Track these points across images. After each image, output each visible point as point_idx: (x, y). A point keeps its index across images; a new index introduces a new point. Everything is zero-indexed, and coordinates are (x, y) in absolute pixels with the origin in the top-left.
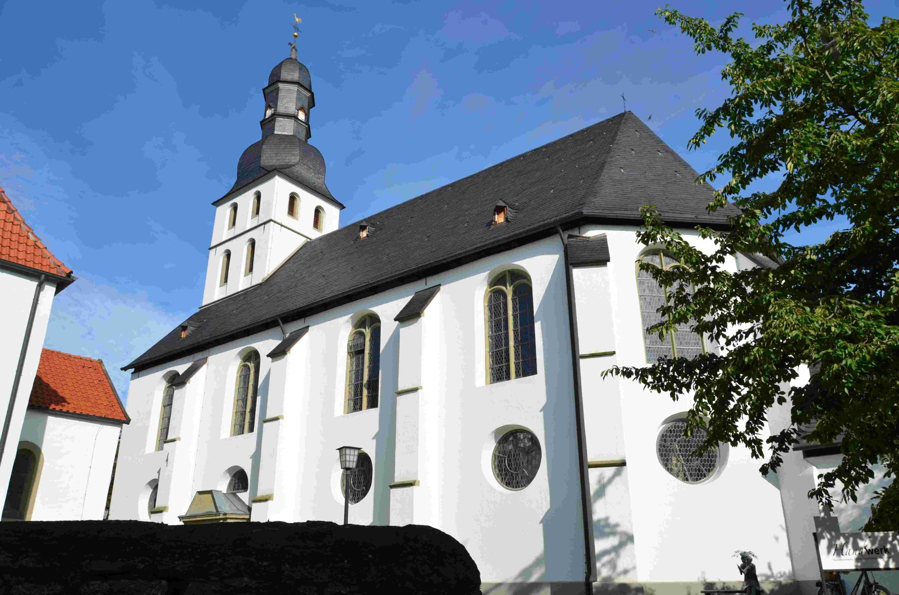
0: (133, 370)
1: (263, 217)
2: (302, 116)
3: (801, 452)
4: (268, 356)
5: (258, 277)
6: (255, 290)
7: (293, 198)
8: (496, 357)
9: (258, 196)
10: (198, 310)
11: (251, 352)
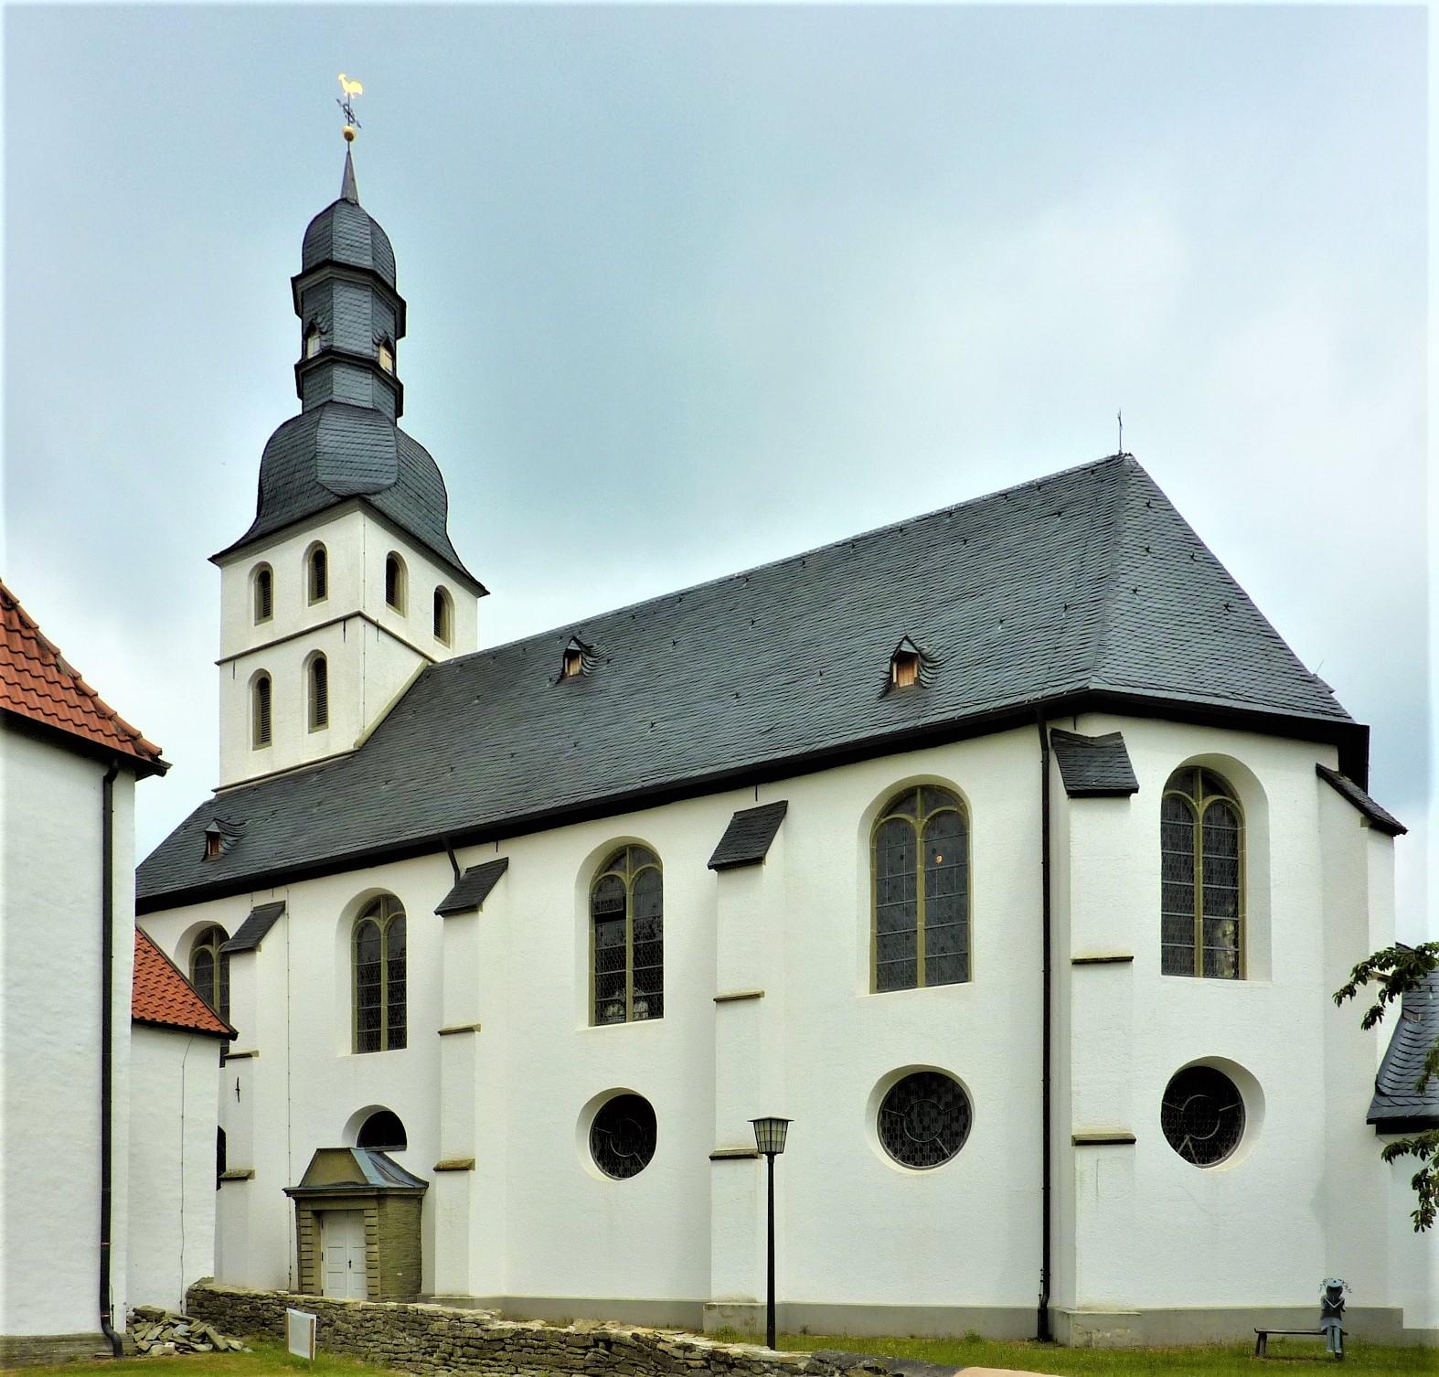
2: (385, 361)
3: (1374, 1126)
5: (343, 735)
7: (393, 566)
9: (318, 558)
10: (212, 796)
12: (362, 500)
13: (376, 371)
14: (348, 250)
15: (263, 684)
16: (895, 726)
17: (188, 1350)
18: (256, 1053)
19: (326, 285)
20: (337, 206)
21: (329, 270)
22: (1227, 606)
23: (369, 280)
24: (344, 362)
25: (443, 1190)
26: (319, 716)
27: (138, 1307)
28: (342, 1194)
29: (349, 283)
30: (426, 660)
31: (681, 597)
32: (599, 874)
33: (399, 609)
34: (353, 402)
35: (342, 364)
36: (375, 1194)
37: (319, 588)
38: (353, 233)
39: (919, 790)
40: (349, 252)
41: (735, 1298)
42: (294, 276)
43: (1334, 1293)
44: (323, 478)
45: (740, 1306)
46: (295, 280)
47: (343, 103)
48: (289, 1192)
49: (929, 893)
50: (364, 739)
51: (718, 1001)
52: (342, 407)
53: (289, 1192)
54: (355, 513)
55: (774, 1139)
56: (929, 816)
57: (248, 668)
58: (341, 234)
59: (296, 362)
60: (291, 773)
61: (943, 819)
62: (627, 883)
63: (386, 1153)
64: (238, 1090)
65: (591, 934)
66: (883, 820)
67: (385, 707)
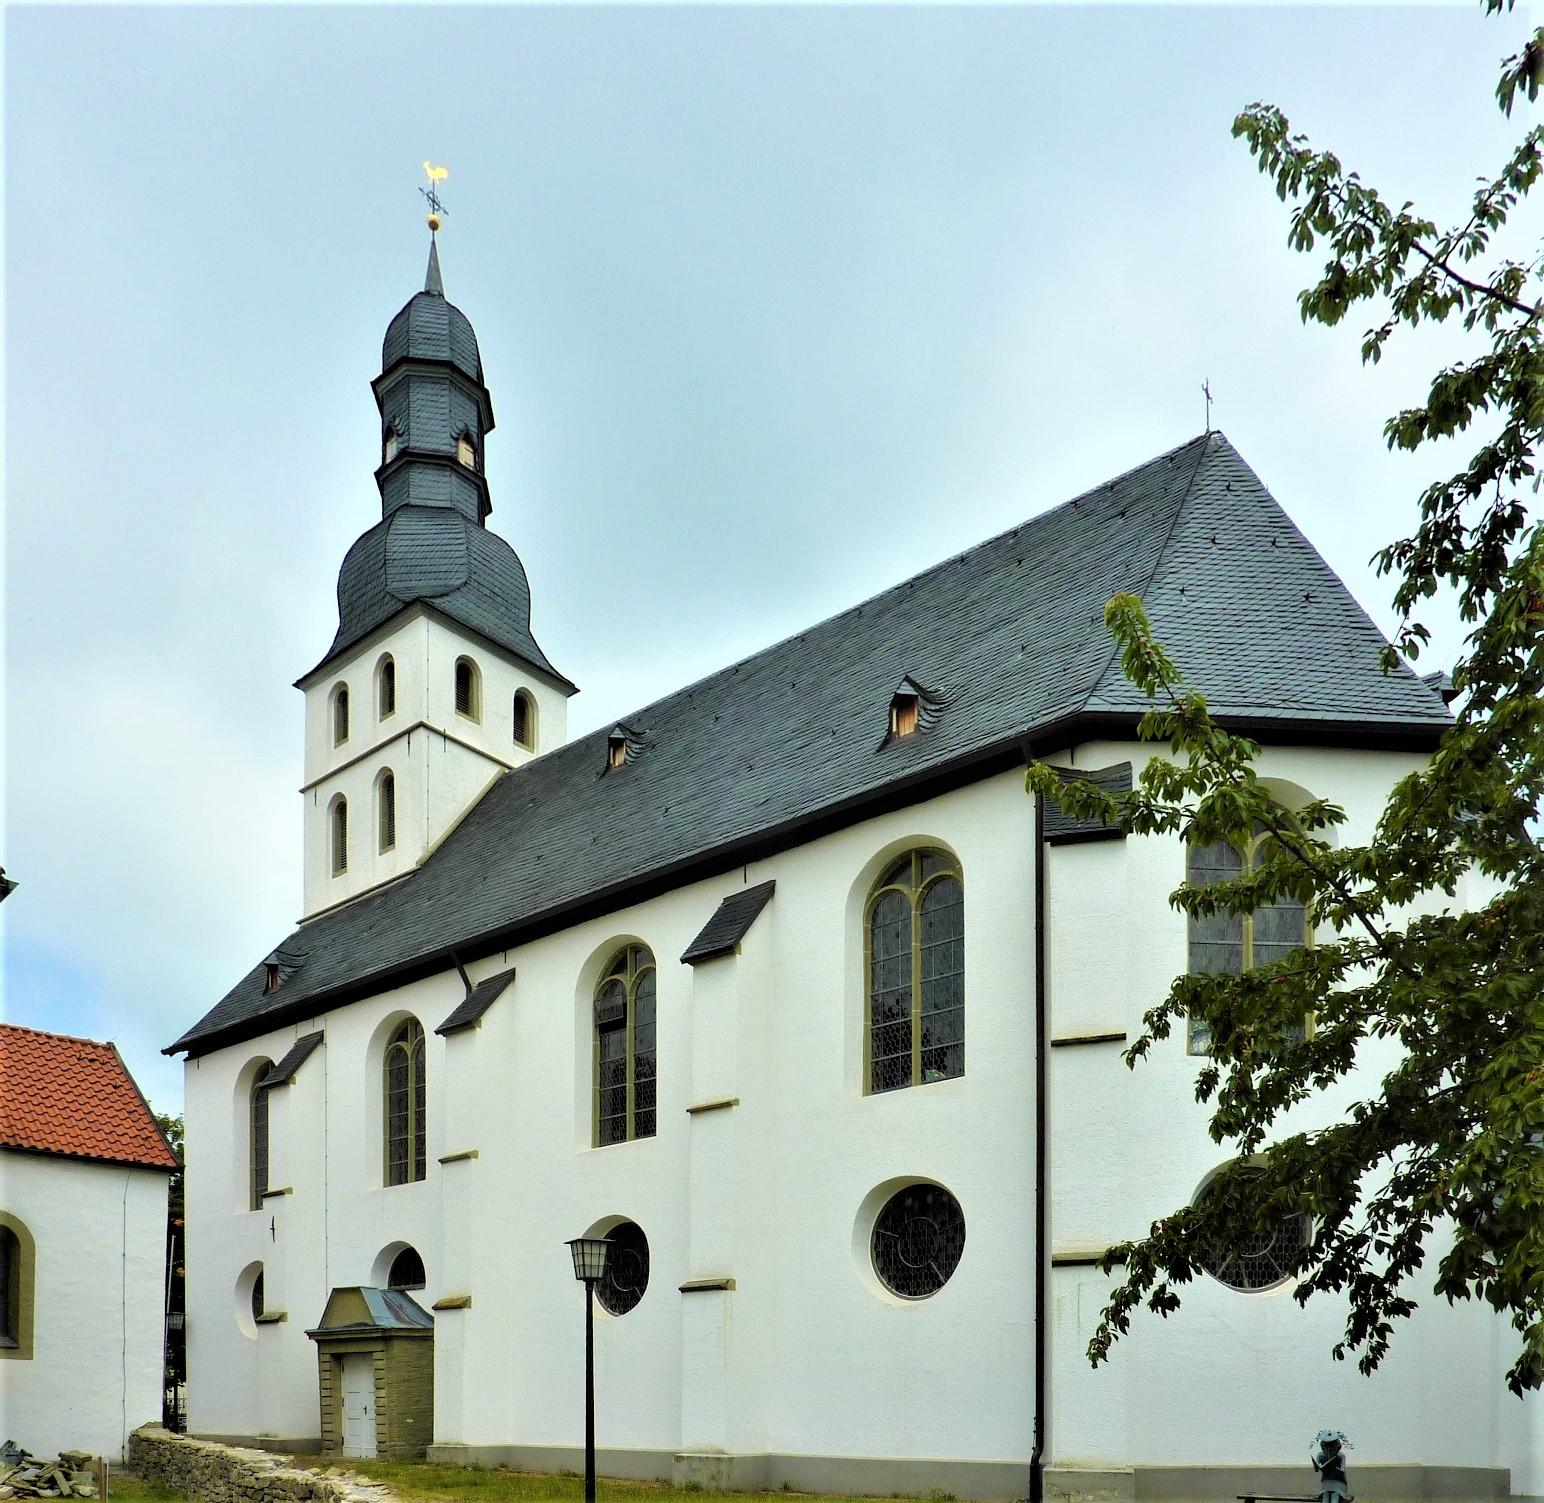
0: (185, 1054)
1: (402, 719)
2: (466, 456)
4: (437, 1032)
5: (407, 856)
6: (403, 885)
7: (465, 673)
8: (885, 1039)
9: (388, 669)
10: (296, 928)
11: (407, 1019)
12: (427, 606)
13: (455, 467)
14: (425, 344)
15: (340, 808)
16: (878, 782)
17: (28, 1495)
18: (290, 1191)
19: (403, 385)
20: (414, 302)
21: (404, 369)
22: (1307, 597)
23: (444, 372)
24: (419, 462)
25: (444, 1327)
26: (388, 839)
27: (65, 1452)
28: (341, 1337)
29: (423, 379)
30: (503, 768)
31: (736, 669)
32: (602, 980)
33: (473, 717)
34: (430, 503)
35: (418, 465)
36: (380, 1335)
37: (388, 704)
38: (430, 325)
39: (913, 854)
40: (426, 346)
41: (704, 1448)
42: (373, 379)
43: (1331, 1447)
44: (393, 586)
45: (707, 1458)
46: (374, 384)
47: (426, 191)
48: (311, 1335)
49: (925, 972)
50: (428, 854)
51: (694, 1112)
52: (415, 510)
53: (311, 1335)
54: (419, 619)
55: (587, 1261)
56: (923, 885)
57: (327, 793)
58: (418, 328)
59: (376, 469)
60: (364, 897)
61: (939, 888)
62: (628, 987)
63: (408, 1293)
64: (273, 1229)
65: (595, 1046)
66: (876, 894)
67: (453, 821)
